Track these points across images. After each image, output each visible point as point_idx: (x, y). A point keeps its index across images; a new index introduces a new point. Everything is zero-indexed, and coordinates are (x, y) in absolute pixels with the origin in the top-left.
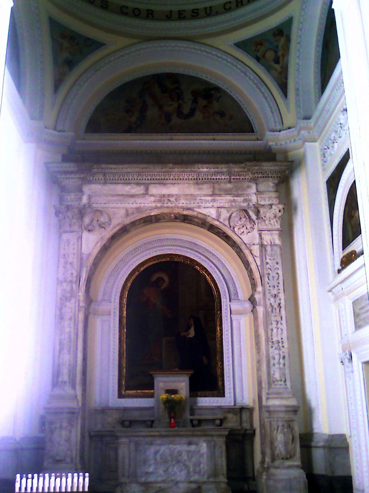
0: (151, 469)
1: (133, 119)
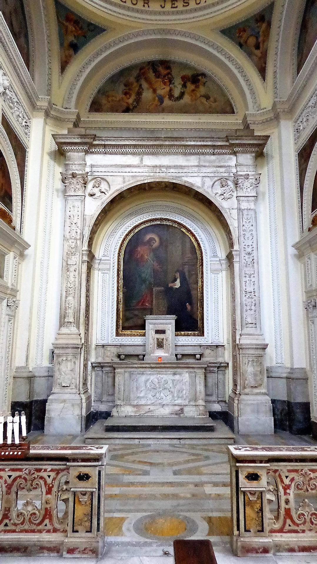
0: (142, 395)
1: (131, 101)
